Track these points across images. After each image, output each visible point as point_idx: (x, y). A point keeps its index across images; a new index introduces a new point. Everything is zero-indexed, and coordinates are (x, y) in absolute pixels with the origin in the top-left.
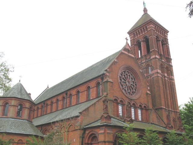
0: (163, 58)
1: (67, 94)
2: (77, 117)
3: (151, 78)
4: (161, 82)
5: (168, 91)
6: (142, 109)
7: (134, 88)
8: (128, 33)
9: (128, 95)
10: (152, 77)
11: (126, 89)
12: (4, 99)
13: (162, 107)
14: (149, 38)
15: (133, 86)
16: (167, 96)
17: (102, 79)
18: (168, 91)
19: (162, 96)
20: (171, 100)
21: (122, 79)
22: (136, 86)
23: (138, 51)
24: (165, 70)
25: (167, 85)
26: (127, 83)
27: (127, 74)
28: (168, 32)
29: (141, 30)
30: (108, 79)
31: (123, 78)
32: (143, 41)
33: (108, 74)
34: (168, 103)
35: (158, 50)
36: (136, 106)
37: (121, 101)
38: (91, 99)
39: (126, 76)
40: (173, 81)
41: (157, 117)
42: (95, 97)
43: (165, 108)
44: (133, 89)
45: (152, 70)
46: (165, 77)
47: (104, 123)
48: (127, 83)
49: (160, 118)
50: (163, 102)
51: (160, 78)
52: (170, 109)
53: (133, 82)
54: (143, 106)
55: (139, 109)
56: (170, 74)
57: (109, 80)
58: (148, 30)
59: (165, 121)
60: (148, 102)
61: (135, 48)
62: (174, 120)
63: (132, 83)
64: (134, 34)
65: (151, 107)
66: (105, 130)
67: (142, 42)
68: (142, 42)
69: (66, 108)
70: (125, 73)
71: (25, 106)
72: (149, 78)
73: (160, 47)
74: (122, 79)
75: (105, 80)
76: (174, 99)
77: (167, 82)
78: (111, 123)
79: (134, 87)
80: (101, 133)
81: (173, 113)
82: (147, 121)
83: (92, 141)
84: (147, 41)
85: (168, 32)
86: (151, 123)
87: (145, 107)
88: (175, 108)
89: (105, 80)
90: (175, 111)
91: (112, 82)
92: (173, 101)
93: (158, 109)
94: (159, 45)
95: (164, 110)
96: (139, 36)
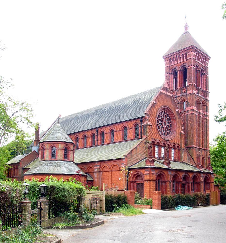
0: (200, 92)
1: (97, 131)
2: (123, 159)
3: (185, 115)
4: (195, 120)
5: (201, 129)
6: (175, 149)
7: (169, 129)
8: (163, 57)
9: (163, 136)
10: (187, 114)
11: (162, 130)
12: (50, 142)
13: (194, 146)
14: (188, 69)
15: (169, 126)
16: (199, 134)
17: (142, 121)
18: (201, 129)
19: (195, 135)
20: (203, 138)
21: (159, 120)
22: (171, 126)
23: (173, 79)
24: (201, 106)
25: (201, 123)
26: (164, 124)
27: (163, 115)
28: (210, 58)
29: (179, 56)
30: (148, 122)
31: (160, 119)
32: (180, 71)
33: (147, 117)
34: (199, 141)
35: (196, 84)
36: (171, 146)
37: (158, 143)
38: (128, 139)
39: (163, 117)
40: (207, 118)
41: (188, 156)
42: (133, 139)
43: (196, 146)
44: (169, 129)
45: (187, 106)
46: (200, 113)
47: (149, 166)
48: (164, 124)
49: (190, 156)
50: (195, 141)
51: (195, 116)
52: (201, 148)
53: (169, 122)
54: (176, 146)
55: (172, 149)
56: (206, 109)
57: (149, 124)
58: (188, 58)
59: (195, 159)
60: (181, 142)
61: (170, 77)
62: (203, 158)
63: (167, 124)
64: (170, 59)
65: (183, 146)
66: (150, 172)
67: (179, 71)
68: (179, 71)
69: (97, 146)
70: (162, 114)
71: (70, 149)
72: (183, 115)
73: (198, 83)
74: (159, 120)
75: (145, 123)
76: (206, 137)
77: (201, 119)
78: (154, 166)
79: (169, 128)
80: (147, 174)
81: (203, 151)
82: (179, 160)
83: (136, 180)
84: (185, 71)
85: (210, 58)
86: (183, 162)
87: (178, 147)
88: (206, 146)
89: (145, 123)
90: (206, 149)
91: (151, 126)
92: (205, 138)
93: (189, 147)
94: (198, 77)
95: (195, 149)
96: (176, 63)
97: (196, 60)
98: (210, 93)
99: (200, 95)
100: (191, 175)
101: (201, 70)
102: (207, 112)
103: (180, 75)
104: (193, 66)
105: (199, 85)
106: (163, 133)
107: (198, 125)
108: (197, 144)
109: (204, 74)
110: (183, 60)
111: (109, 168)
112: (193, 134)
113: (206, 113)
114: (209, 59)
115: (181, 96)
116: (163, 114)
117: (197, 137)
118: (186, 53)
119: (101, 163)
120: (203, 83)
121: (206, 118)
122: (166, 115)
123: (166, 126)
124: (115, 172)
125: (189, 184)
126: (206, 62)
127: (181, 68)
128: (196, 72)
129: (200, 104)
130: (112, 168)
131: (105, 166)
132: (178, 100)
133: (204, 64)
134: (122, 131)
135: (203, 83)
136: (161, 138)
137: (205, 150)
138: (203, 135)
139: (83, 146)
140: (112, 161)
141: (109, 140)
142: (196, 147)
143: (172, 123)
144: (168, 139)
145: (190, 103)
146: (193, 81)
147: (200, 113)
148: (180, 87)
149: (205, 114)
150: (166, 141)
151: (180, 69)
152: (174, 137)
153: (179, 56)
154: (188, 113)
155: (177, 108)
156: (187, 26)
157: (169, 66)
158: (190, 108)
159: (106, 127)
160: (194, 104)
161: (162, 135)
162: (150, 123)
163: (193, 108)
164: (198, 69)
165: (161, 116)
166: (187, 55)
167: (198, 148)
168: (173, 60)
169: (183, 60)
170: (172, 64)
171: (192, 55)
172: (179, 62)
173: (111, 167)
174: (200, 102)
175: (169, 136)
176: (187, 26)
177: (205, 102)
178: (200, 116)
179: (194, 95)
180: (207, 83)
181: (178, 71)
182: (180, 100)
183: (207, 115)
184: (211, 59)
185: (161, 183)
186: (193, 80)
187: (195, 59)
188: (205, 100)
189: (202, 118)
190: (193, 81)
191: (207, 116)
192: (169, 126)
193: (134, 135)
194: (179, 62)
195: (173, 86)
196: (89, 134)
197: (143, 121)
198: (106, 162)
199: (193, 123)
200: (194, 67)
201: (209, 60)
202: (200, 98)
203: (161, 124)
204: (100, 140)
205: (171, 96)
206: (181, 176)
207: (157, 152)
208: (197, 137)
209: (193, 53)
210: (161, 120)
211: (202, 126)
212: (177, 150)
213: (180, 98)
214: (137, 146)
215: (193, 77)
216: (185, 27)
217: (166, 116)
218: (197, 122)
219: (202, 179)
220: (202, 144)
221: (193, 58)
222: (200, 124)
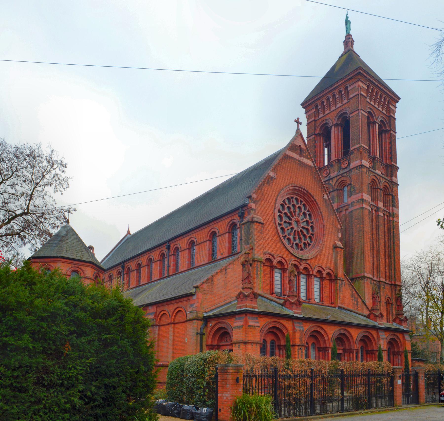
0: (378, 164)
3: (347, 212)
4: (367, 222)
6: (322, 279)
7: (308, 236)
8: (301, 105)
9: (294, 251)
10: (350, 210)
11: (291, 237)
13: (366, 275)
14: (350, 113)
15: (307, 230)
16: (378, 251)
22: (313, 231)
24: (380, 194)
25: (381, 228)
26: (294, 225)
28: (399, 99)
30: (255, 216)
31: (285, 214)
32: (336, 125)
38: (219, 258)
39: (292, 210)
40: (395, 219)
43: (371, 276)
46: (378, 209)
48: (294, 225)
50: (368, 265)
52: (383, 279)
53: (307, 221)
56: (391, 201)
58: (351, 96)
61: (318, 142)
65: (341, 272)
72: (343, 213)
77: (381, 221)
84: (345, 124)
85: (399, 99)
90: (393, 283)
91: (262, 224)
96: (327, 112)
97: (368, 100)
98: (399, 170)
99: (378, 172)
100: (356, 334)
101: (378, 122)
102: (394, 208)
103: (335, 134)
104: (361, 109)
105: (375, 151)
106: (293, 243)
107: (374, 232)
108: (373, 273)
110: (342, 103)
111: (169, 316)
112: (364, 250)
113: (393, 210)
114: (398, 102)
115: (339, 175)
116: (293, 202)
117: (373, 257)
118: (346, 88)
119: (157, 307)
120: (384, 148)
121: (393, 219)
122: (299, 205)
123: (301, 228)
124: (180, 325)
125: (351, 354)
126: (391, 106)
127: (338, 119)
128: (369, 126)
129: (379, 190)
130: (175, 316)
131: (163, 312)
132: (333, 185)
133: (386, 111)
134: (208, 243)
135: (386, 150)
136: (287, 253)
137: (392, 285)
138: (387, 253)
139: (148, 280)
140: (175, 301)
141: (187, 262)
142: (369, 278)
143: (314, 223)
144: (305, 256)
145: (357, 186)
146: (361, 141)
147: (377, 207)
148: (336, 158)
149: (391, 211)
150: (299, 260)
151: (335, 122)
152: (318, 253)
153: (334, 96)
154: (353, 208)
155: (324, 192)
156: (350, 40)
157: (315, 121)
158: (355, 197)
159: (182, 237)
160: (365, 188)
161: (292, 247)
162: (260, 218)
163: (362, 196)
164: (373, 119)
165: (289, 208)
166: (348, 91)
167: (376, 281)
168: (321, 106)
169: (342, 103)
170: (321, 116)
171: (359, 88)
172: (333, 108)
173: (172, 315)
174: (379, 185)
175: (307, 250)
176: (349, 38)
177: (388, 186)
178: (378, 215)
179: (364, 170)
180: (392, 144)
181: (331, 127)
182: (337, 183)
183: (393, 213)
184: (400, 101)
185: (279, 351)
186: (361, 139)
187: (364, 96)
188: (390, 183)
189: (384, 219)
190: (361, 141)
191: (395, 216)
192: (307, 230)
193: (229, 247)
195: (322, 159)
196: (155, 255)
197: (246, 215)
198: (165, 303)
199: (363, 228)
200: (362, 112)
201: (397, 104)
202: (378, 177)
203: (288, 225)
204: (173, 264)
205: (311, 167)
206: (330, 336)
207: (280, 284)
208: (373, 257)
209: (361, 84)
210: (289, 214)
211: (385, 236)
212: (328, 281)
213: (336, 180)
214: (226, 267)
215: (361, 134)
216: (347, 42)
217: (299, 208)
218: (373, 226)
219: (383, 344)
220: (386, 272)
221: (361, 94)
222: (379, 232)
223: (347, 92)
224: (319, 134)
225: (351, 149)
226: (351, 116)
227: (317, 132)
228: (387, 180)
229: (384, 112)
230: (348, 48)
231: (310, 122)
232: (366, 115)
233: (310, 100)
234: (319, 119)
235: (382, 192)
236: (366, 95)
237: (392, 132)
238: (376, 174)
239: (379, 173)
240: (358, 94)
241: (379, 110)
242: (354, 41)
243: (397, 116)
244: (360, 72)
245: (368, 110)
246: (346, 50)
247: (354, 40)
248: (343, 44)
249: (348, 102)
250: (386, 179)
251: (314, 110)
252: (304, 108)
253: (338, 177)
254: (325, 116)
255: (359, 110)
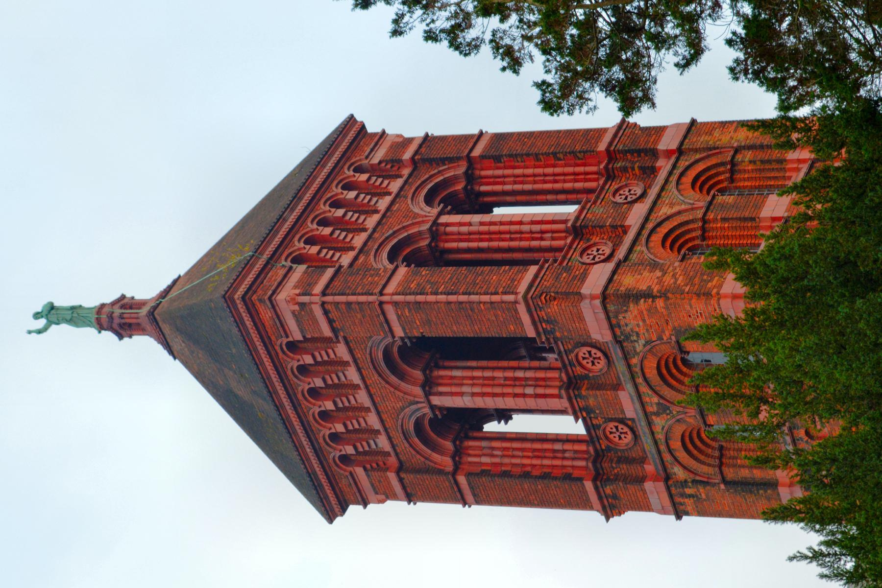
8: (331, 520)
28: (351, 119)
32: (429, 386)
58: (327, 332)
67: (436, 401)
84: (430, 353)
85: (351, 119)
96: (373, 420)
99: (635, 216)
104: (381, 293)
109: (470, 177)
114: (363, 127)
118: (293, 346)
127: (402, 376)
148: (563, 392)
151: (418, 391)
157: (400, 469)
169: (368, 410)
170: (383, 442)
176: (111, 316)
181: (433, 407)
184: (359, 118)
188: (683, 163)
194: (363, 398)
200: (390, 289)
201: (371, 129)
221: (324, 293)
223: (340, 414)
224: (458, 454)
225: (531, 333)
226: (399, 332)
227: (447, 462)
228: (670, 173)
229: (395, 186)
230: (146, 323)
231: (404, 488)
232: (403, 270)
233: (311, 475)
234: (397, 454)
235: (720, 199)
236: (330, 272)
237: (476, 152)
238: (642, 227)
239: (639, 211)
240: (323, 304)
241: (388, 209)
242: (123, 297)
243: (415, 131)
244: (243, 298)
245: (386, 262)
246: (149, 327)
247: (117, 296)
248: (126, 340)
249: (347, 343)
250: (667, 181)
251: (359, 471)
252: (343, 510)
253: (644, 388)
254: (367, 387)
255: (381, 303)
